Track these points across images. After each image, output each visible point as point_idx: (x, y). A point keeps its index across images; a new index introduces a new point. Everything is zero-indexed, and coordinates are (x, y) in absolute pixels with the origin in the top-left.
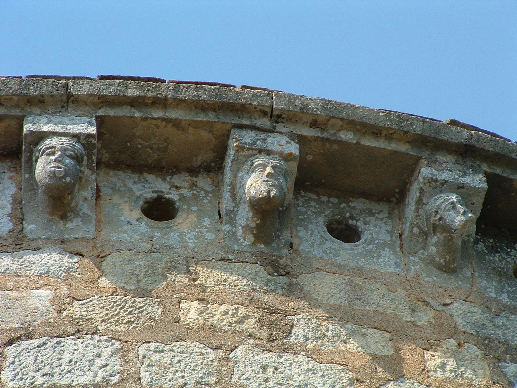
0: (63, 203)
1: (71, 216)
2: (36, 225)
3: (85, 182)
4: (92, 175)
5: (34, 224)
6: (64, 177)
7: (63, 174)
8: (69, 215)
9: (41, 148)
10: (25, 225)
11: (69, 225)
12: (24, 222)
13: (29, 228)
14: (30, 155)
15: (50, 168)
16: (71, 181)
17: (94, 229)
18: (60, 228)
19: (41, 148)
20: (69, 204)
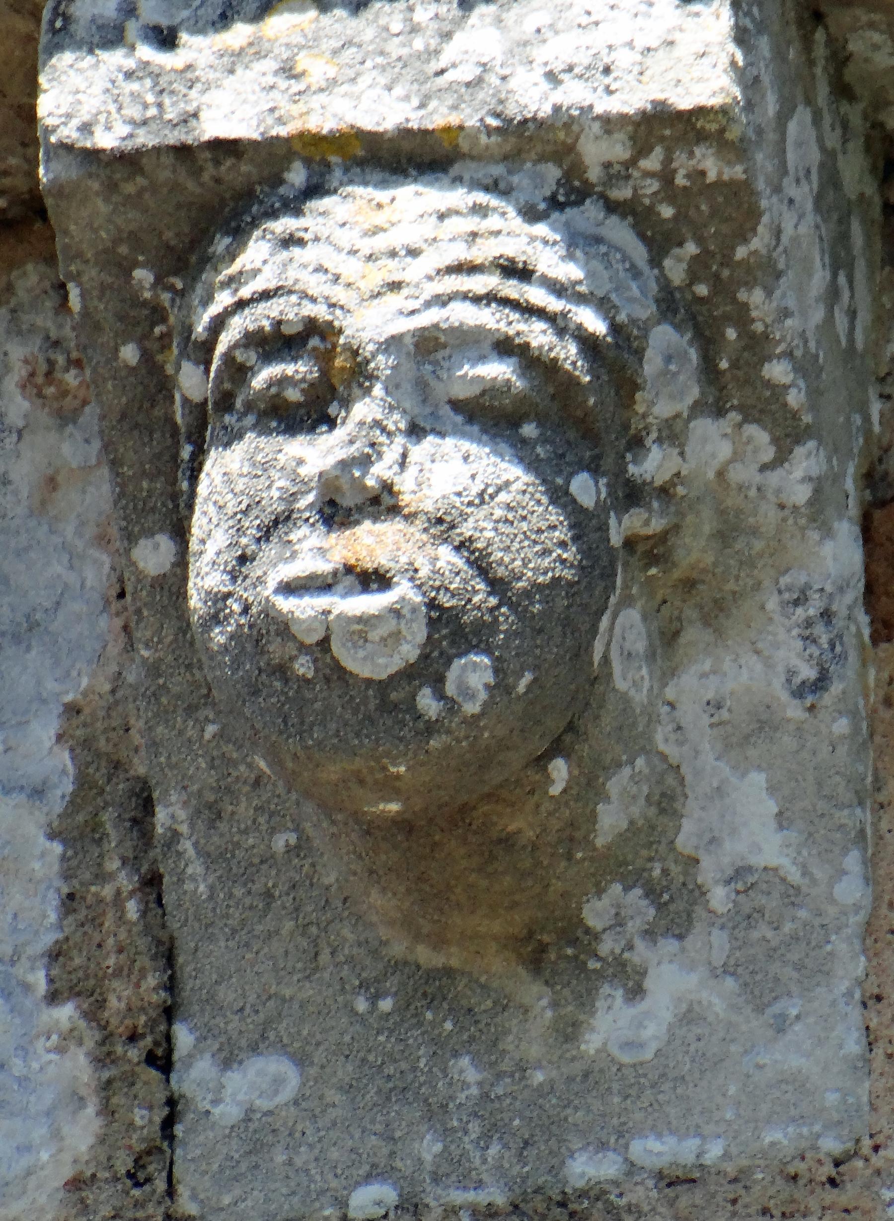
0: (507, 842)
1: (619, 922)
2: (301, 1060)
3: (724, 536)
4: (781, 459)
5: (282, 1048)
6: (428, 670)
7: (409, 652)
8: (595, 913)
9: (218, 324)
10: (196, 1074)
11: (613, 1026)
12: (184, 1037)
13: (228, 1112)
14: (146, 356)
15: (289, 588)
16: (501, 686)
17: (854, 1045)
18: (522, 1068)
19: (218, 324)
20: (575, 832)
